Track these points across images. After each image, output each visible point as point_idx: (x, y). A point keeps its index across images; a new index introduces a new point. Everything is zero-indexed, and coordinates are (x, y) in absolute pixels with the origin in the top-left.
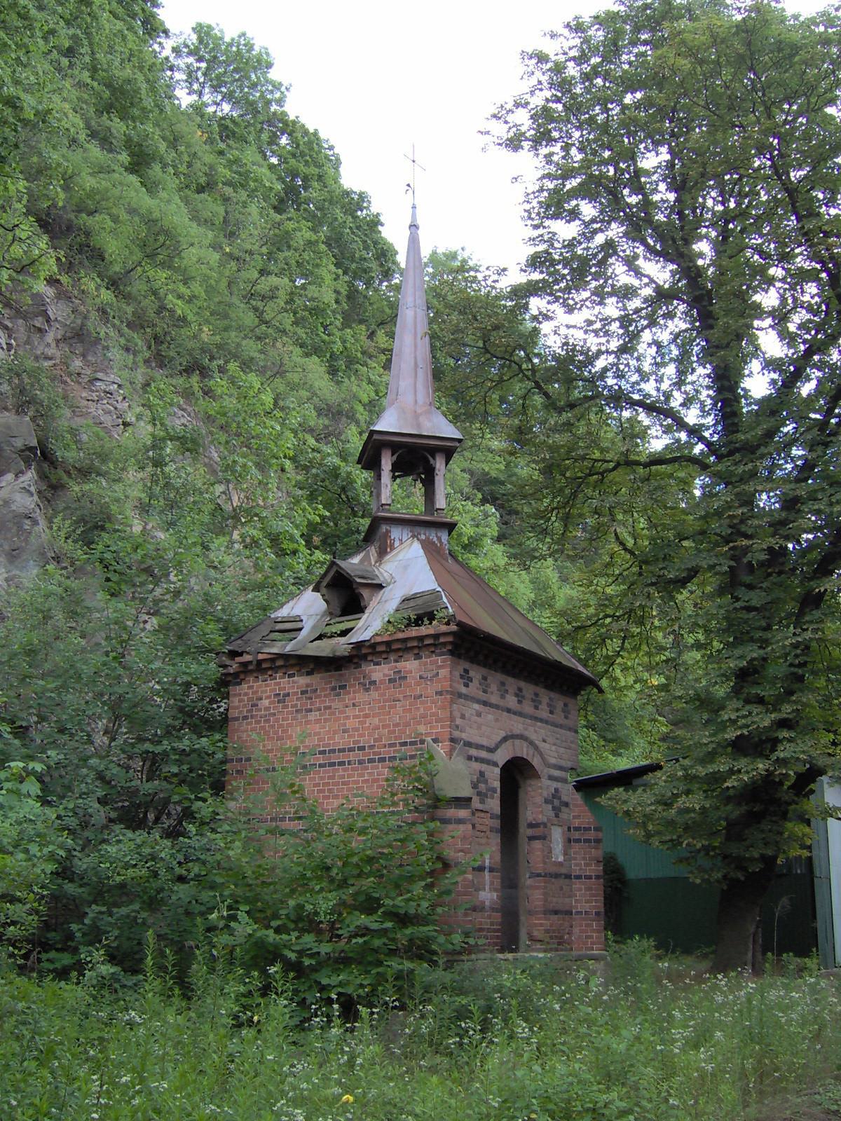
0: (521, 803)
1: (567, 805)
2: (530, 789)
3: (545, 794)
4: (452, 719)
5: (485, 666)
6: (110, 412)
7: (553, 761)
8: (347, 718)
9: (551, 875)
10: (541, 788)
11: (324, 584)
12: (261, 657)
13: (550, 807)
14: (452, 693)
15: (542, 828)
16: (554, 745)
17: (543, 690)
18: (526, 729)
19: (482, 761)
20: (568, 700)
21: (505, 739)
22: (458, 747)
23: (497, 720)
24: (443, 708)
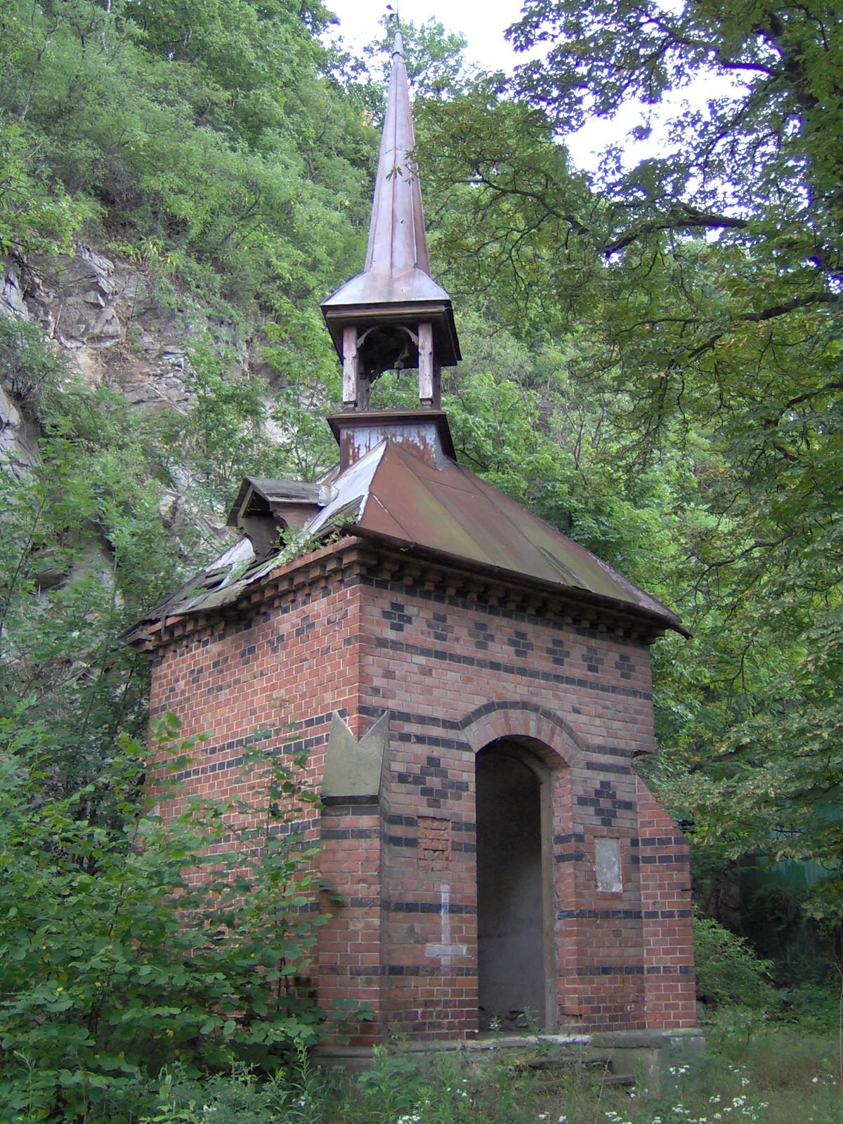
0: (543, 805)
1: (629, 806)
2: (557, 784)
3: (580, 790)
4: (363, 678)
5: (440, 599)
6: (176, 386)
7: (597, 741)
8: (255, 692)
9: (594, 914)
10: (571, 782)
11: (241, 513)
12: (170, 621)
13: (591, 810)
14: (361, 639)
15: (573, 842)
16: (599, 716)
17: (572, 636)
18: (536, 694)
19: (435, 741)
20: (628, 650)
21: (488, 708)
22: (377, 721)
23: (468, 680)
24: (351, 663)
